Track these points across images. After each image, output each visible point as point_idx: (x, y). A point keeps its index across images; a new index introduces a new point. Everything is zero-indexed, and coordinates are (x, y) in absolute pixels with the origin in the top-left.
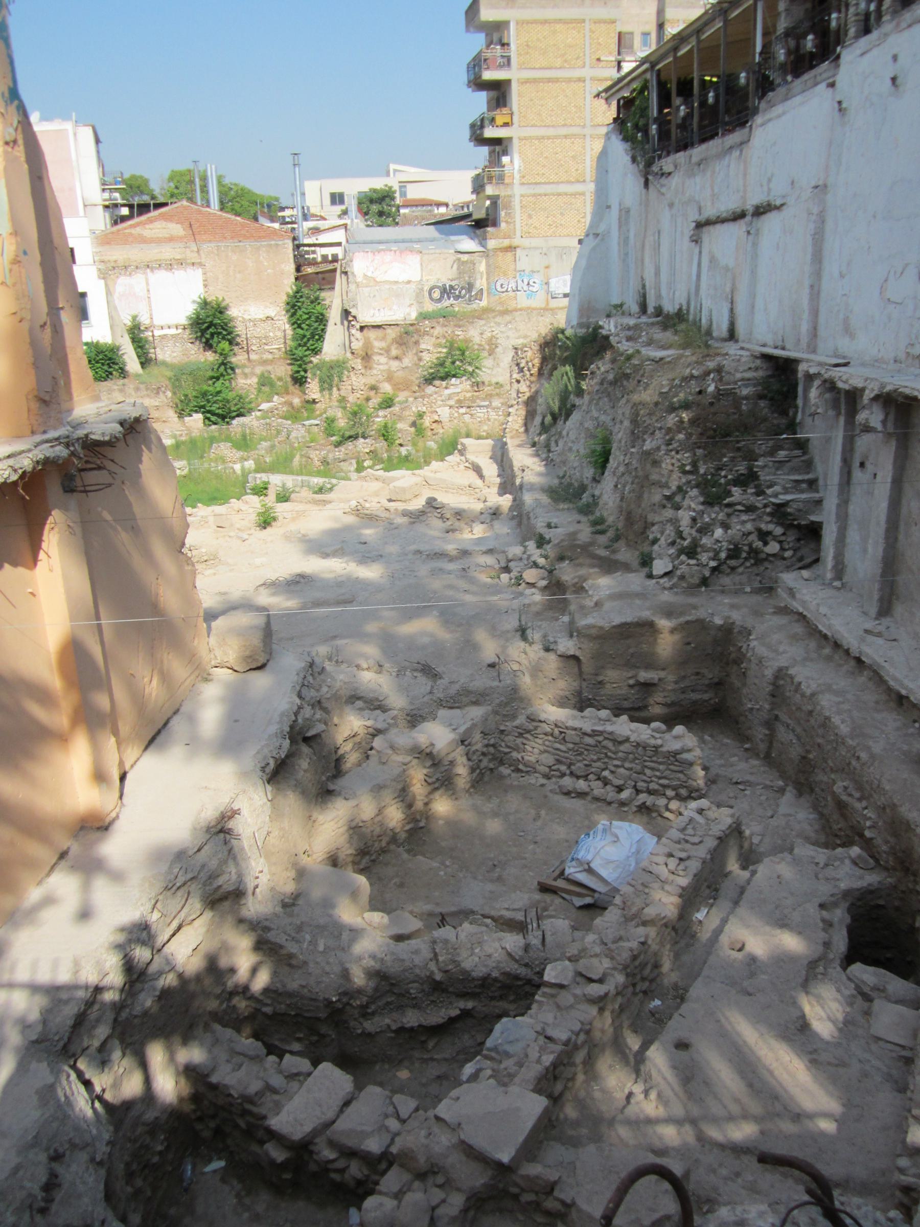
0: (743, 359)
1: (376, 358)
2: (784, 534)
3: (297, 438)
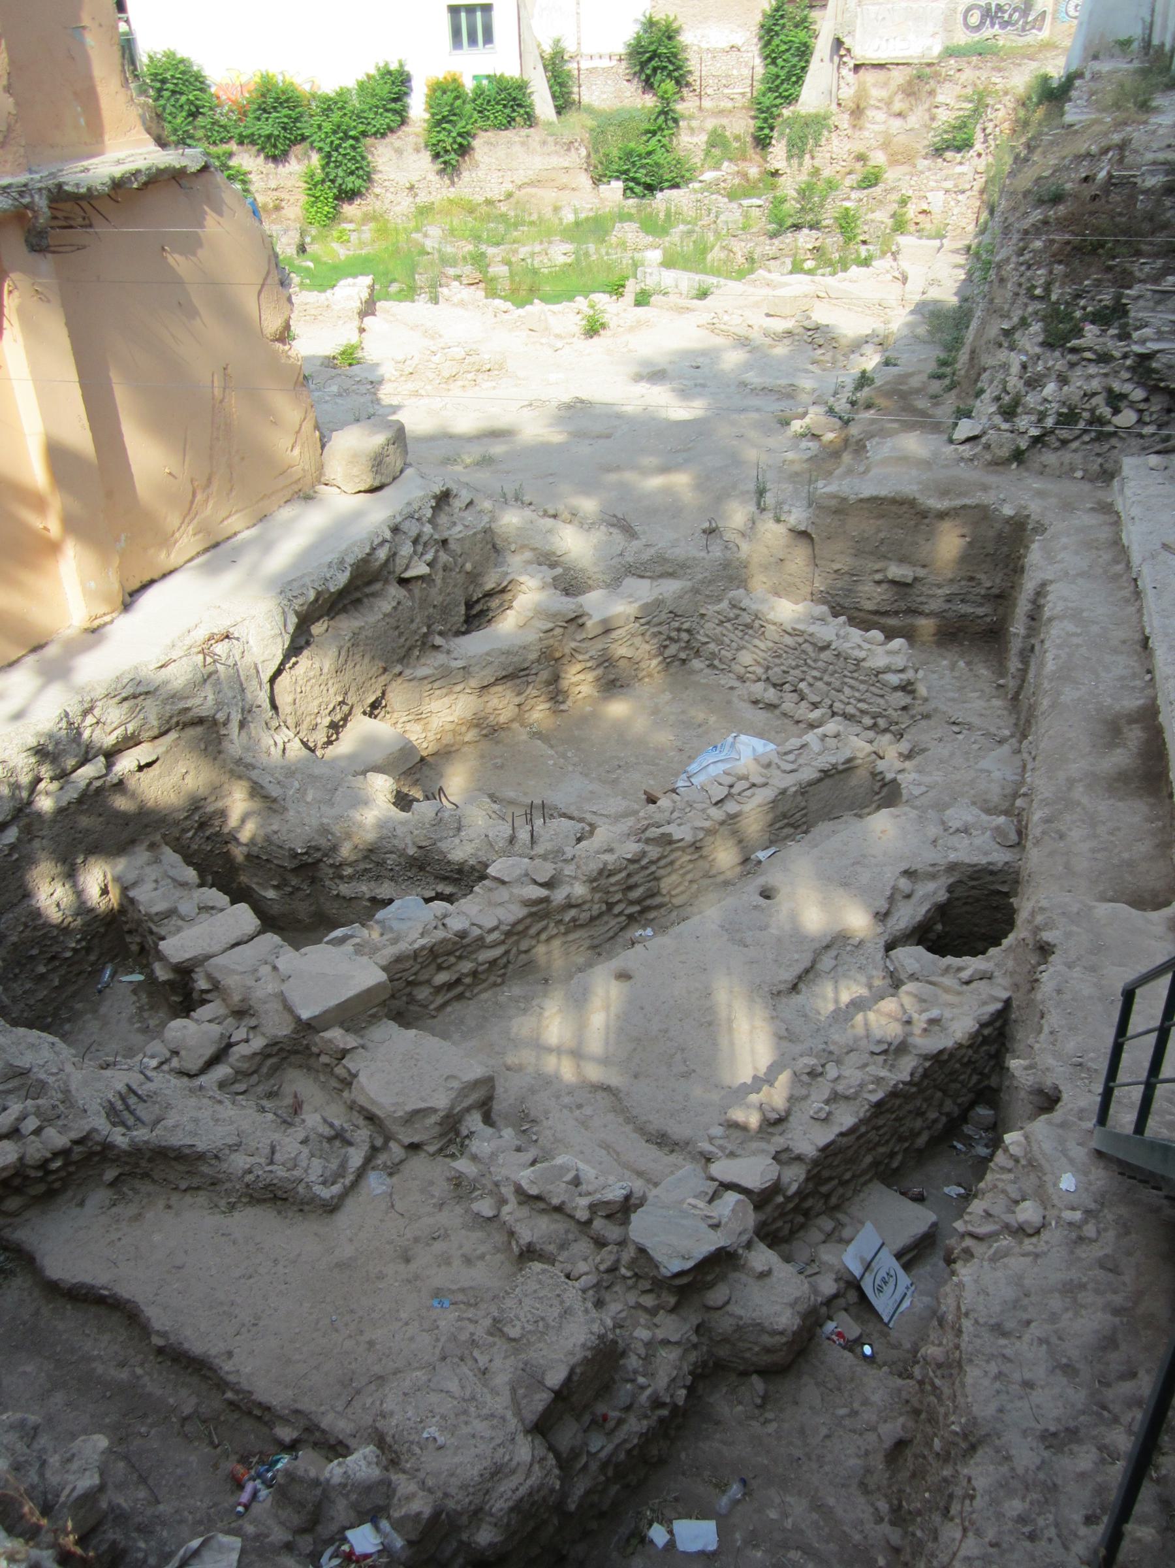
0: (1161, 132)
1: (870, 113)
2: (1146, 400)
3: (726, 222)
